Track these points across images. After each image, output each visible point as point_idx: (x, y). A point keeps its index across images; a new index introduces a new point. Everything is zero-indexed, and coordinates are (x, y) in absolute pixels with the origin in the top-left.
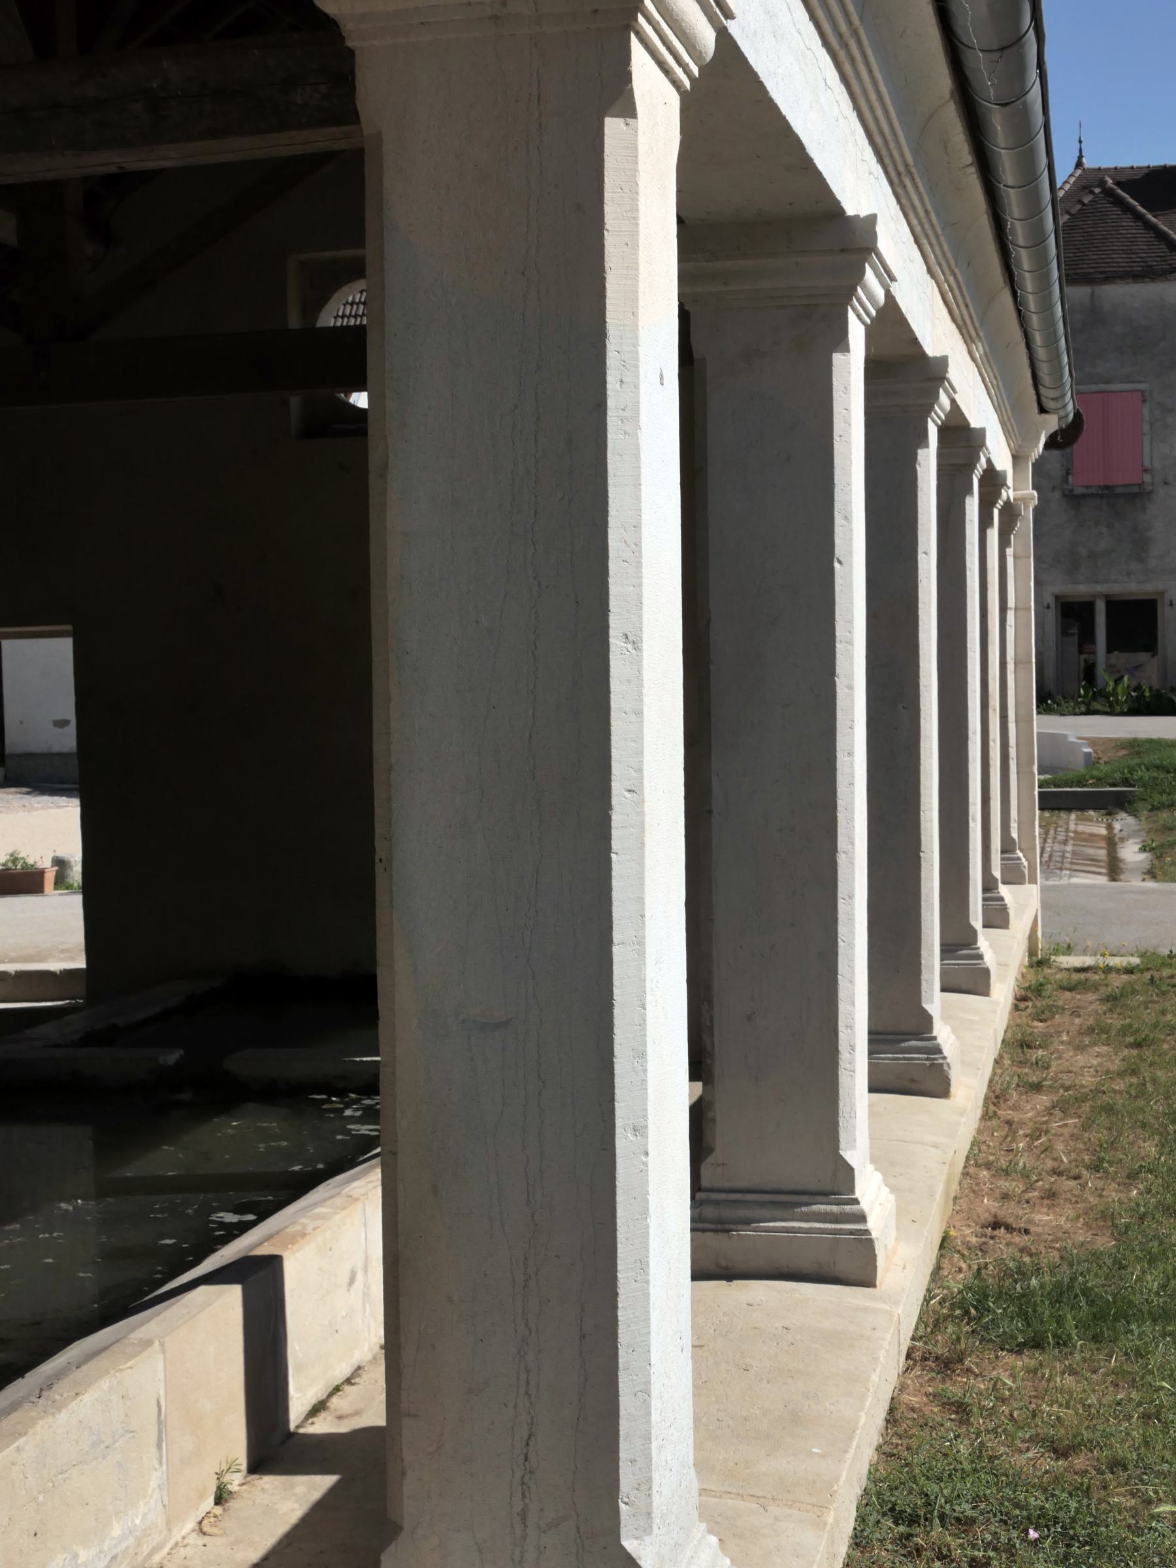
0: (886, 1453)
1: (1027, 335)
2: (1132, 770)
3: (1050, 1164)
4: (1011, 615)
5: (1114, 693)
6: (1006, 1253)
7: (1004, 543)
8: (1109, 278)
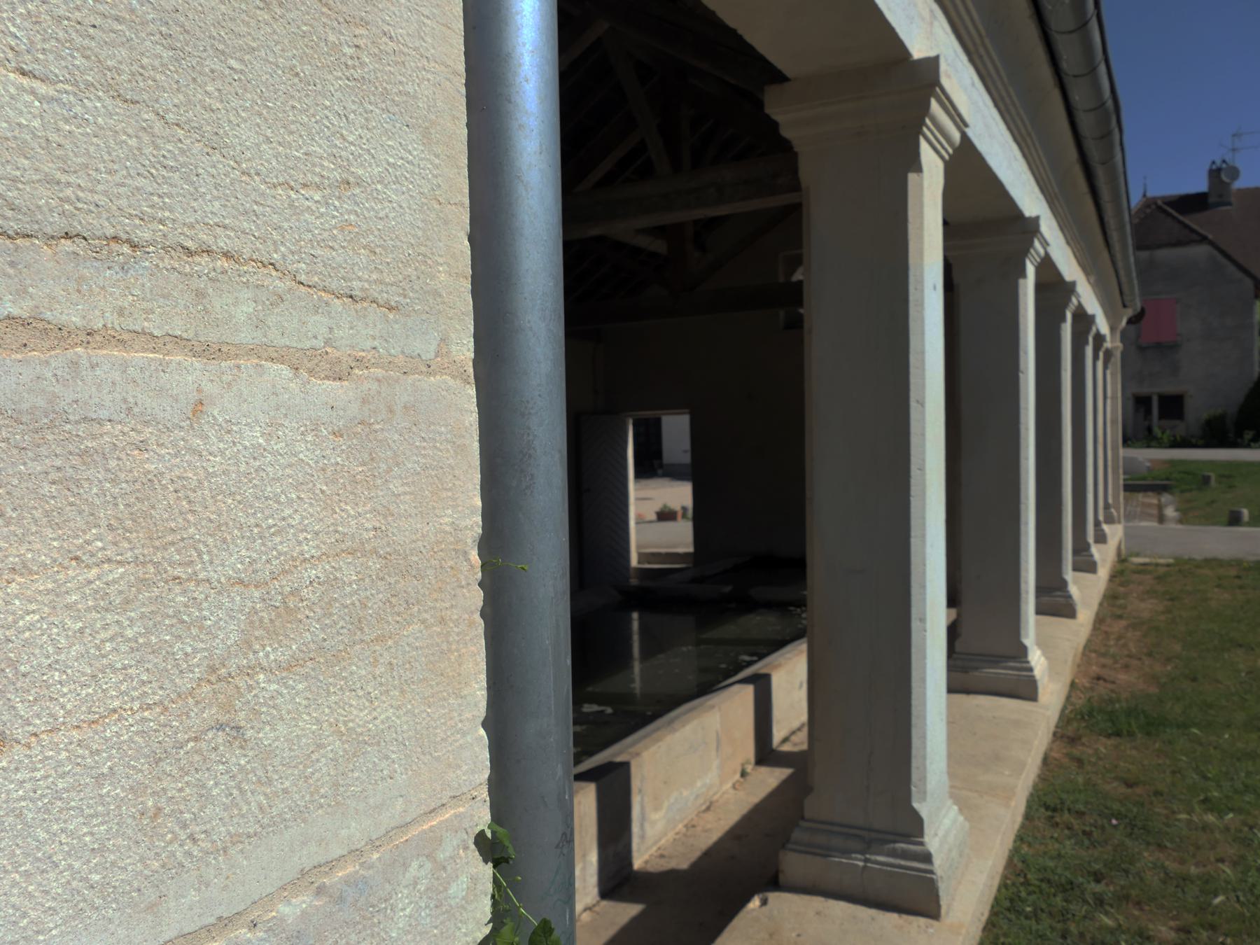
0: (1042, 778)
3: (1126, 652)
4: (1109, 402)
7: (1105, 367)
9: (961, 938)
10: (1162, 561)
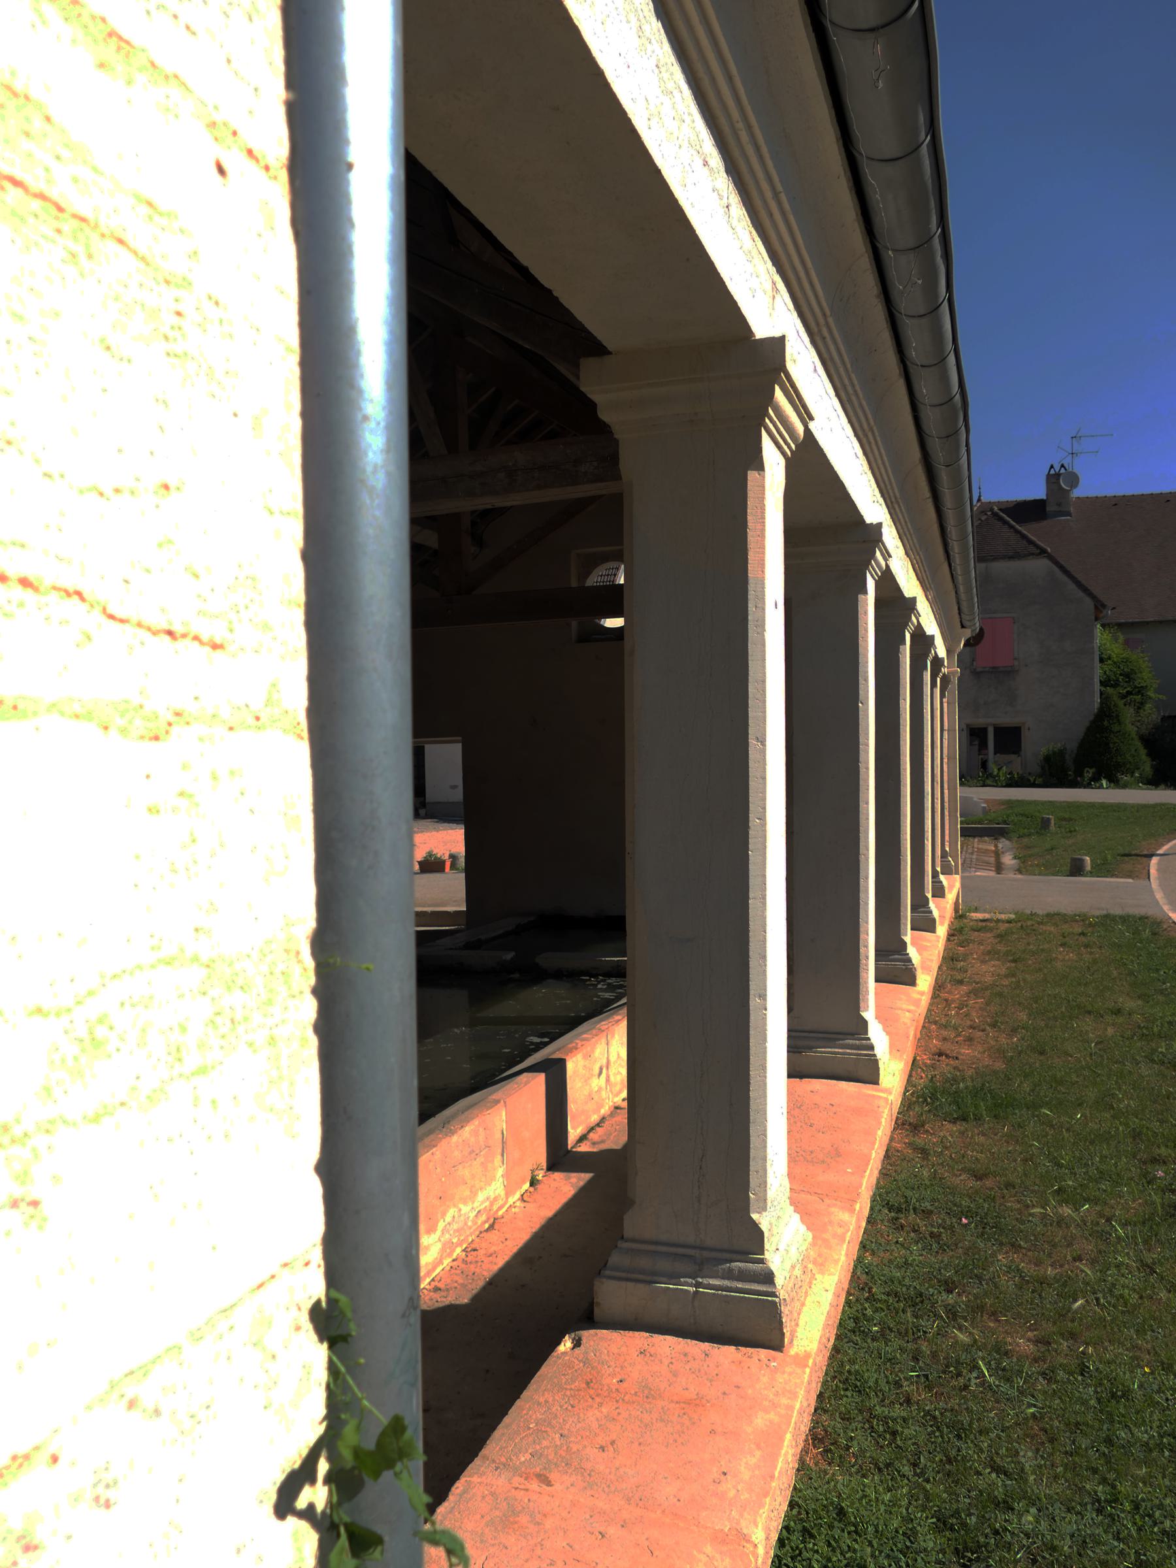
0: (884, 1174)
1: (956, 587)
2: (1008, 816)
3: (969, 1023)
4: (946, 734)
5: (998, 775)
6: (946, 1069)
7: (942, 696)
9: (808, 1370)
10: (1003, 916)
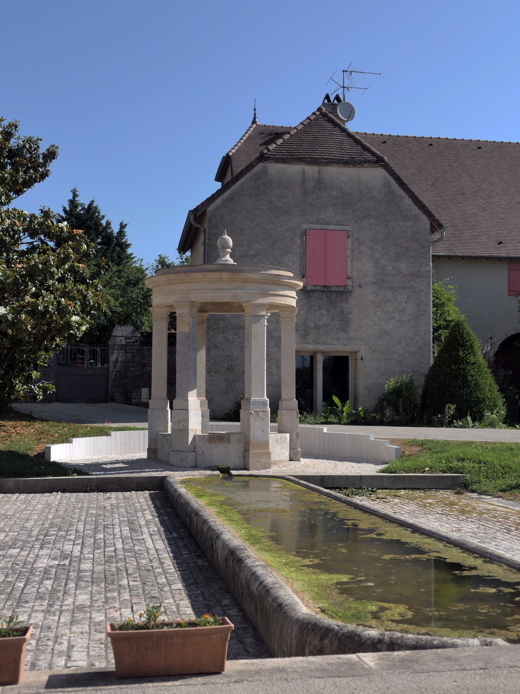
8: (329, 162)
